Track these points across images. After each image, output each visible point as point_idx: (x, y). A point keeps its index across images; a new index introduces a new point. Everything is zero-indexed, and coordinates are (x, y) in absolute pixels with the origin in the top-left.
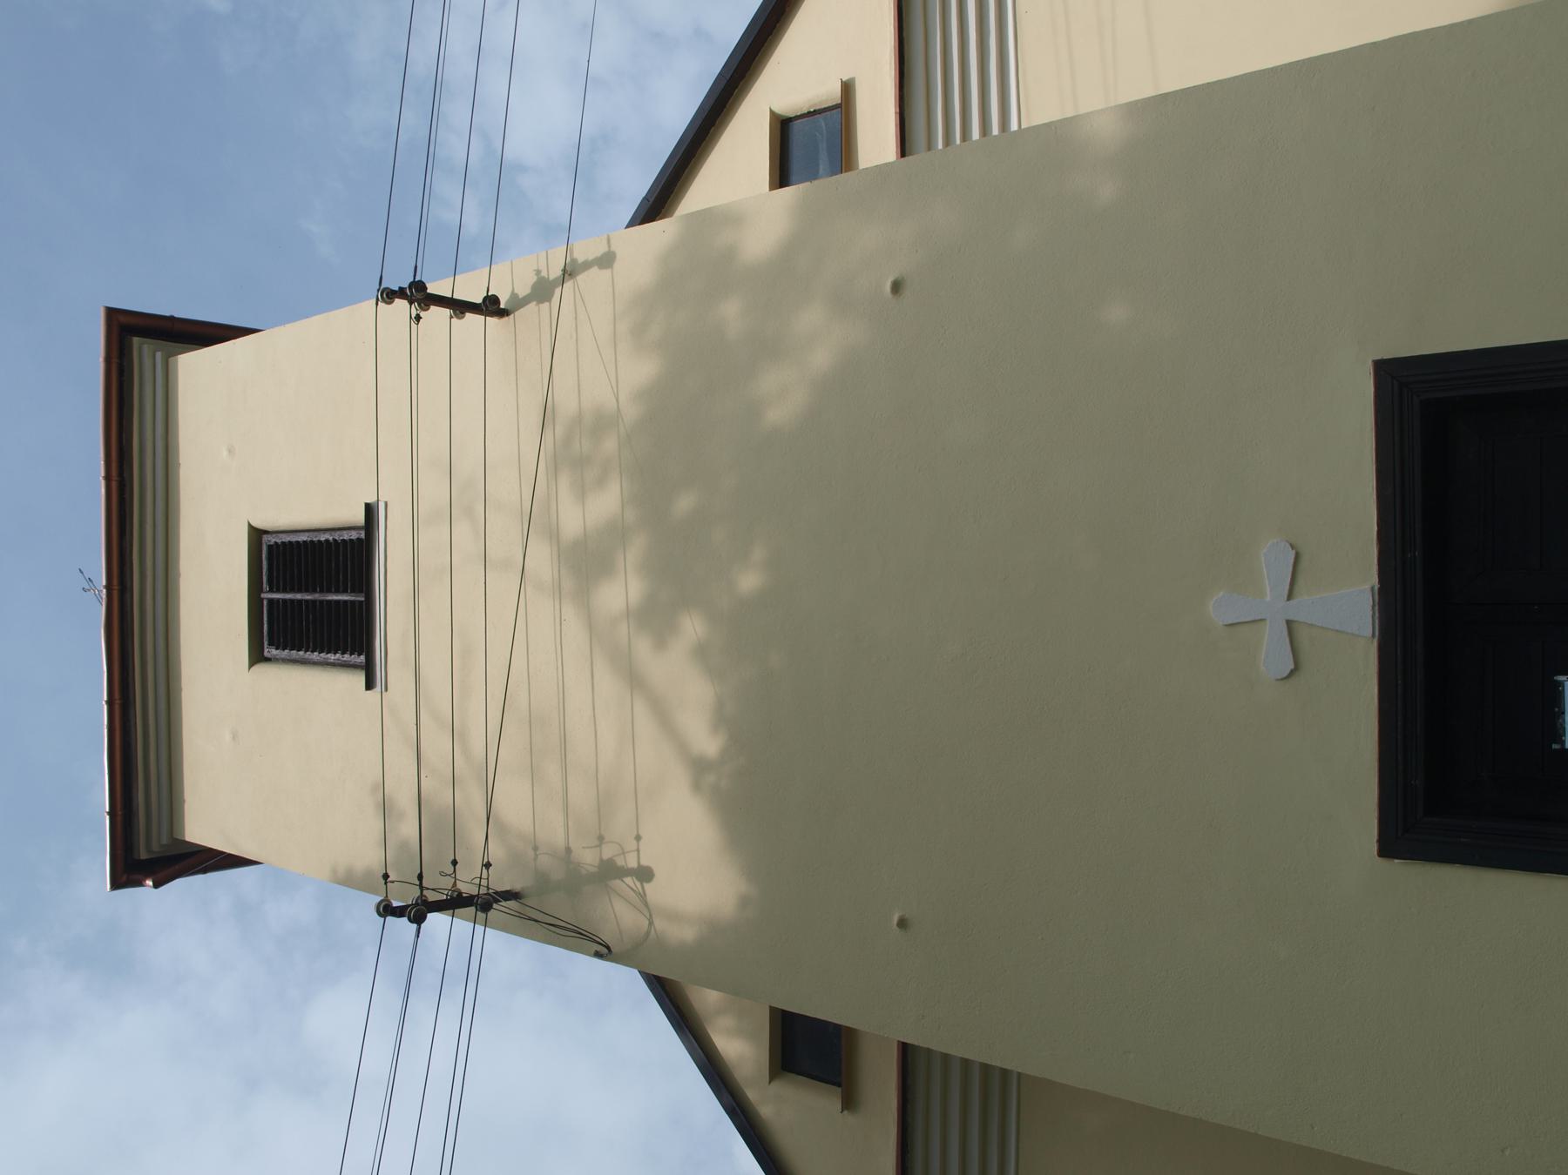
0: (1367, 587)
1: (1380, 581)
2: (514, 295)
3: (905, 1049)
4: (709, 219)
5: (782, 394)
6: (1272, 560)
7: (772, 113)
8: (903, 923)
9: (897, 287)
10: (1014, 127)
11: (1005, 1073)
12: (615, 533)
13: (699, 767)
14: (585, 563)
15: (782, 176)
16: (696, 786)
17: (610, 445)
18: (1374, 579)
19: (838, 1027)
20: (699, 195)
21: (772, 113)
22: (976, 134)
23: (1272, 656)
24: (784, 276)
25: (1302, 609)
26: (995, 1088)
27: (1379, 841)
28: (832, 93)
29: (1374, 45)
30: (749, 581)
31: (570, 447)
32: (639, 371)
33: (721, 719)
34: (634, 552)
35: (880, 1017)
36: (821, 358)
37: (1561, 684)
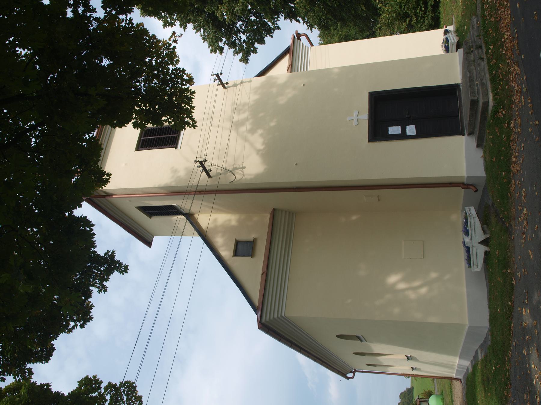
2: (255, 51)
4: (271, 77)
5: (282, 100)
6: (355, 113)
8: (296, 164)
9: (304, 85)
12: (246, 120)
13: (258, 151)
14: (236, 125)
16: (258, 154)
17: (247, 107)
20: (271, 73)
23: (355, 122)
24: (285, 86)
25: (359, 117)
30: (273, 124)
31: (237, 108)
32: (254, 97)
33: (264, 143)
34: (251, 121)
36: (290, 95)
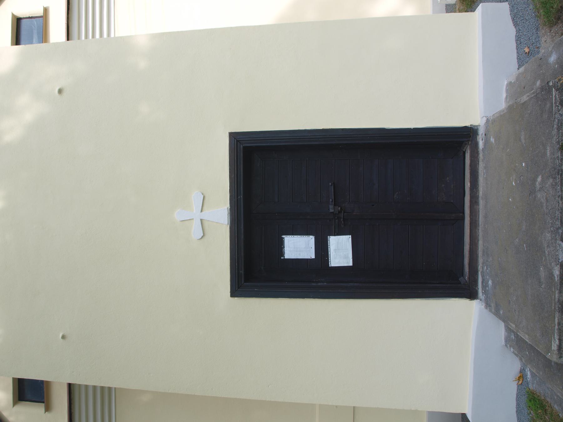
0: (226, 208)
1: (230, 206)
3: (70, 385)
6: (196, 199)
7: (13, 16)
8: (63, 337)
9: (60, 91)
10: (112, 35)
11: (110, 389)
15: (17, 41)
18: (228, 205)
19: (42, 382)
21: (13, 16)
22: (105, 35)
23: (196, 232)
25: (206, 215)
26: (106, 395)
27: (231, 292)
28: (40, 12)
29: (231, 28)
35: (58, 376)
36: (28, 117)
37: (283, 238)
